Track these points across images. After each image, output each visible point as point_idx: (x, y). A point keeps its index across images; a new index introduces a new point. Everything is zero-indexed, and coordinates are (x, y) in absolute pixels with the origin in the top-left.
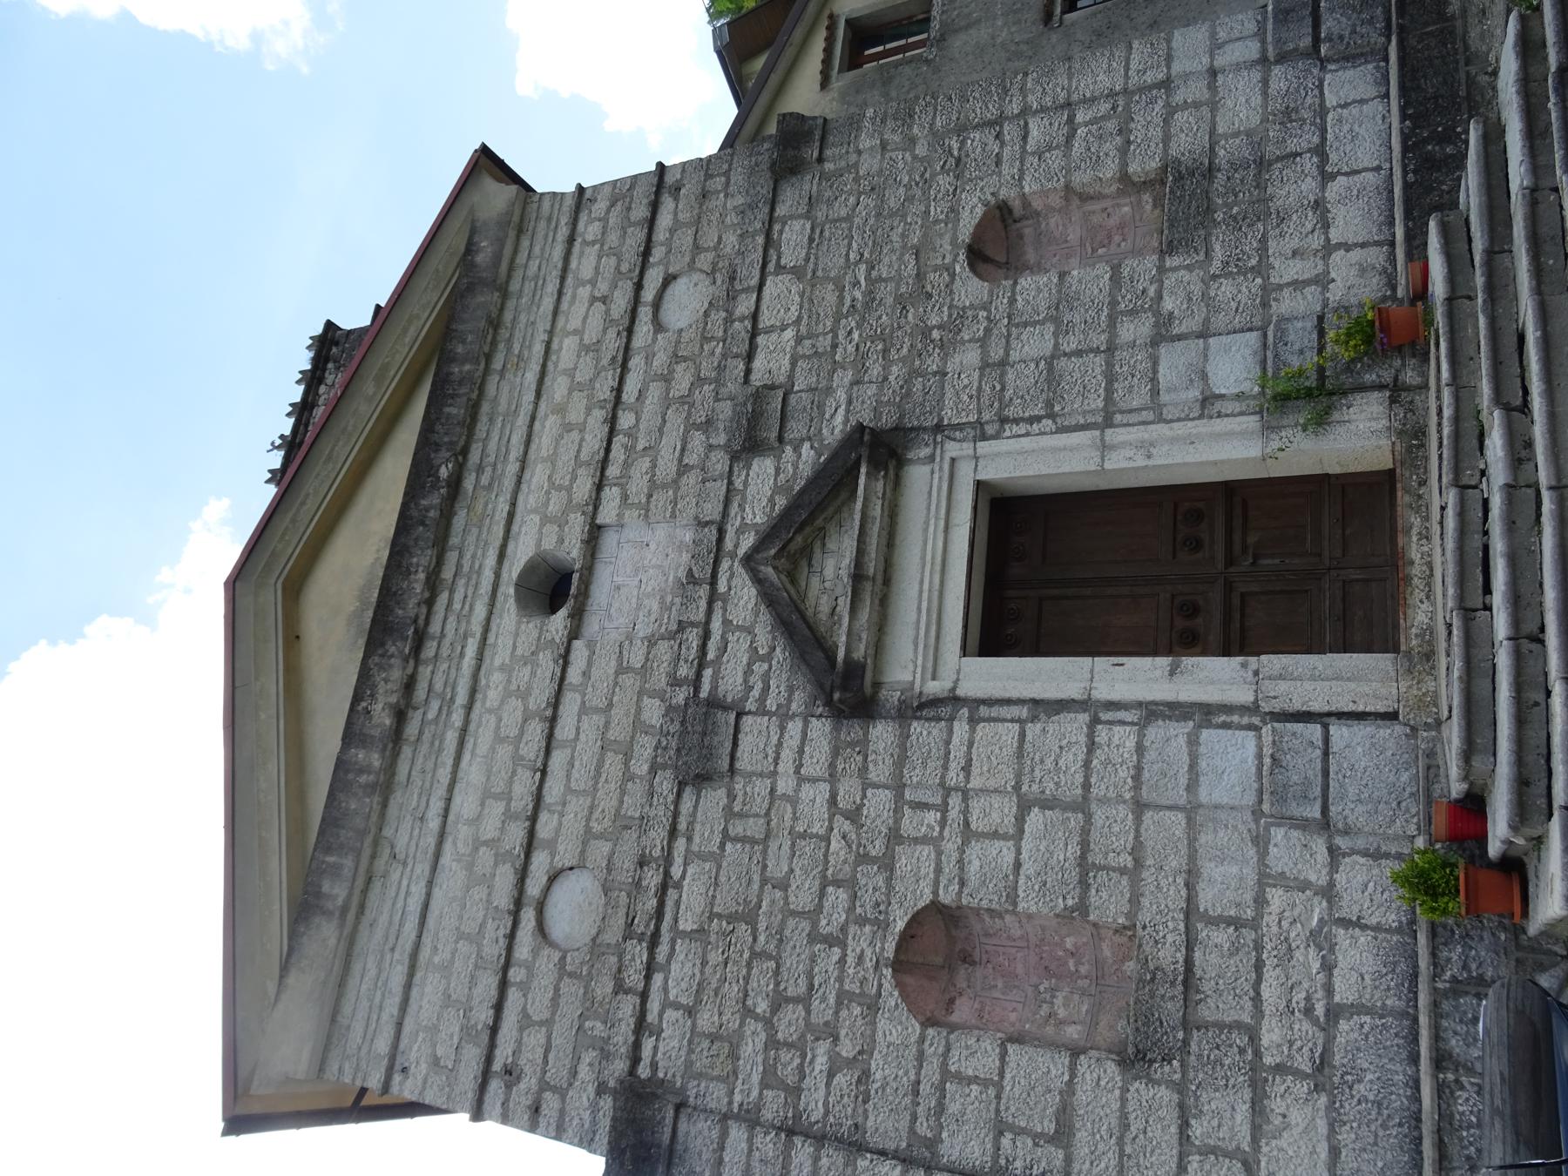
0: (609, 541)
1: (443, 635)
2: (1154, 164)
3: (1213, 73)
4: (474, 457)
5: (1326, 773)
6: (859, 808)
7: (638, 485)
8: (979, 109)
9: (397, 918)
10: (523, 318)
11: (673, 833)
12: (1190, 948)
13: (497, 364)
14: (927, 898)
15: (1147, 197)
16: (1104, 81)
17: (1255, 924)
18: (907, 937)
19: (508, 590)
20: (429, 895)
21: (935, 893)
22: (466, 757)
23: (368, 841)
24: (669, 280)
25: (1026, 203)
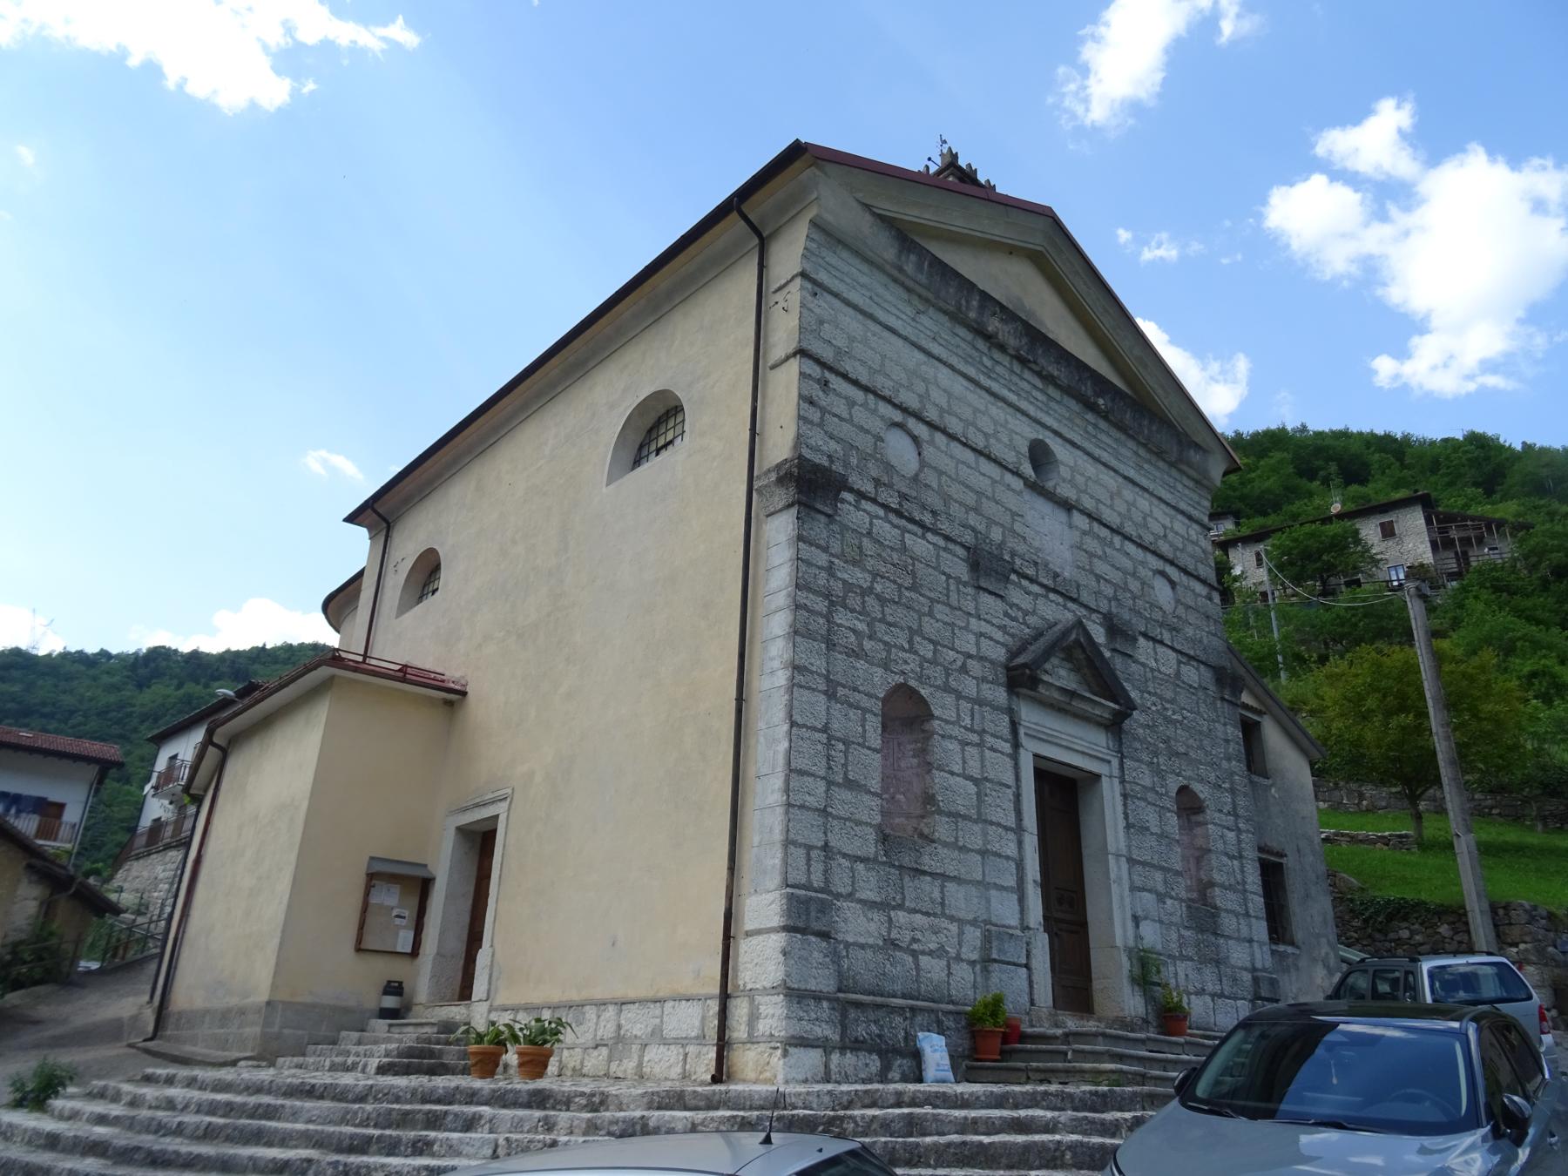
0: (1062, 515)
1: (1022, 379)
2: (1218, 903)
3: (1250, 941)
4: (1103, 424)
5: (1008, 963)
6: (967, 673)
7: (1092, 545)
8: (1241, 802)
9: (886, 305)
10: (1158, 474)
11: (947, 538)
12: (931, 874)
13: (1142, 452)
14: (937, 713)
15: (1195, 895)
16: (1250, 879)
17: (943, 915)
18: (913, 693)
19: (1043, 435)
20: (900, 336)
21: (938, 718)
22: (965, 383)
23: (931, 296)
24: (1173, 584)
25: (1199, 824)
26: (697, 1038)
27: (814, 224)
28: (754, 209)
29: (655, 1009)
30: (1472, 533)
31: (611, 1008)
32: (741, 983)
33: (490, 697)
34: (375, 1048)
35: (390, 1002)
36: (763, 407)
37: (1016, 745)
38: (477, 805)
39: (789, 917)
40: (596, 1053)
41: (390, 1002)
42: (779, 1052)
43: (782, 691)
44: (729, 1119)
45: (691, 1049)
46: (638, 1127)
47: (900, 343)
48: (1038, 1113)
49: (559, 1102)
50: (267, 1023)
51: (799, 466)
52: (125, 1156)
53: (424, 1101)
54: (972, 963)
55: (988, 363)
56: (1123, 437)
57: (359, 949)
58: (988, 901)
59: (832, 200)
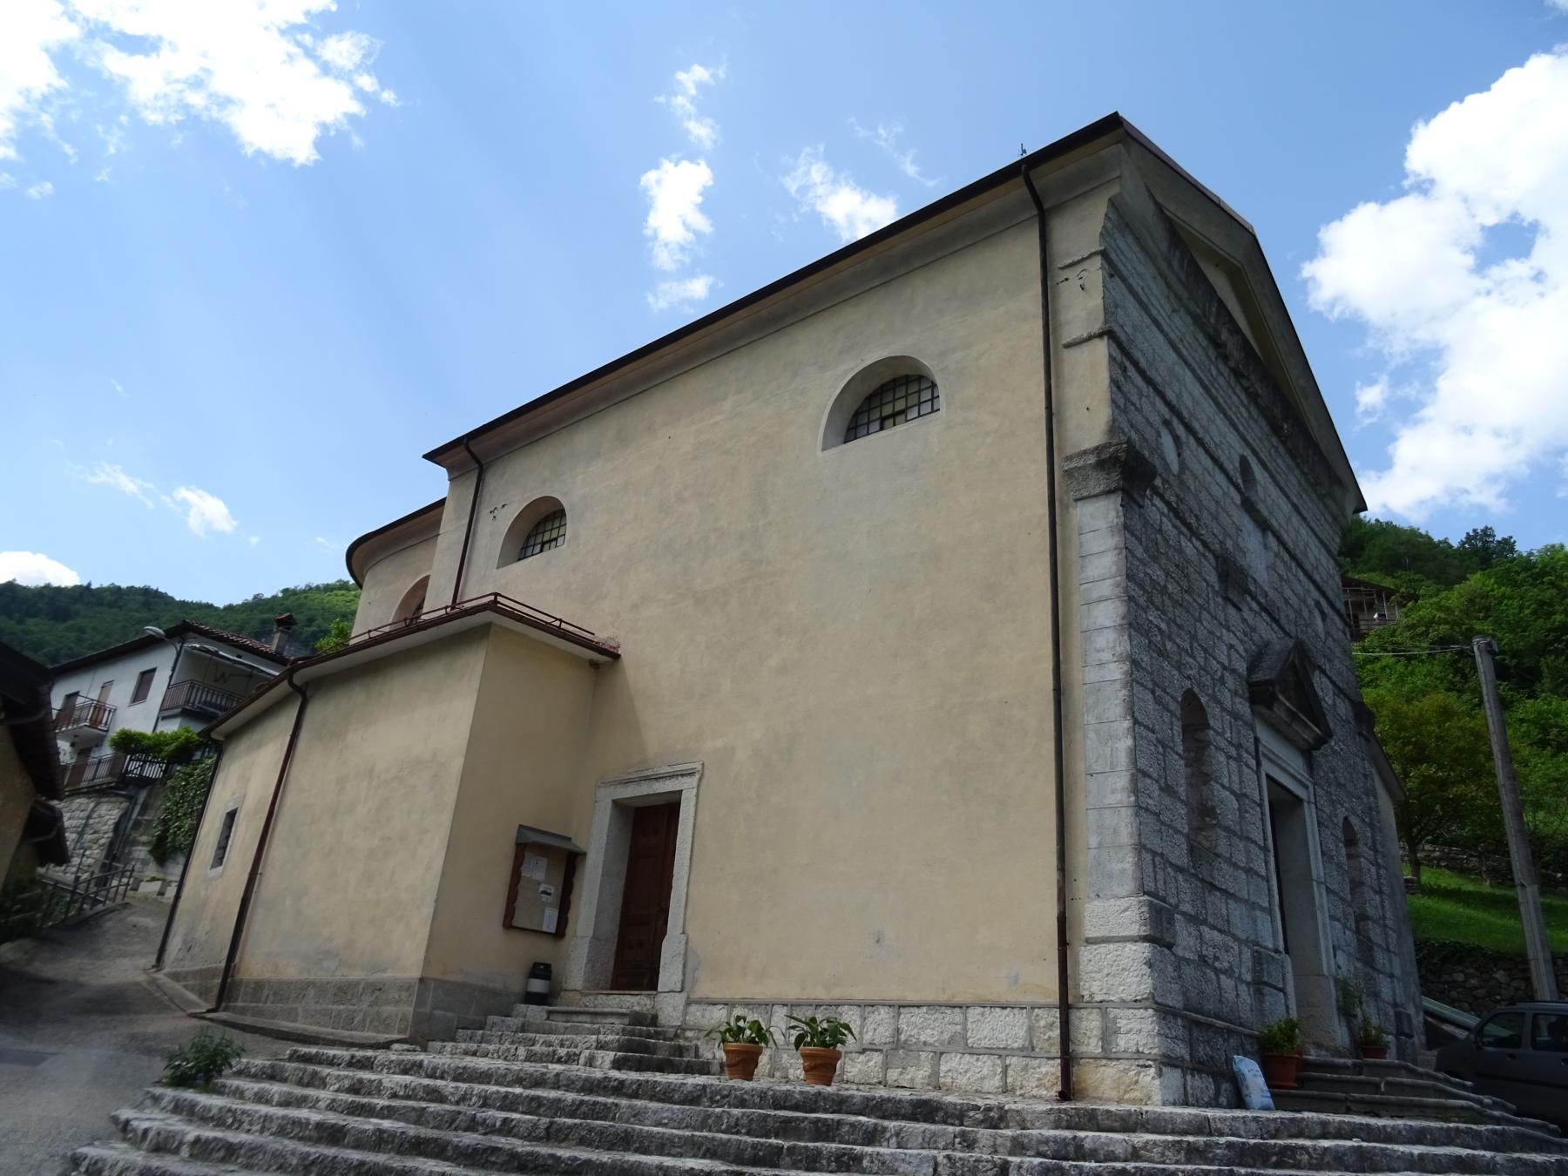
26: (1022, 1049)
27: (1112, 203)
28: (1045, 177)
29: (957, 1015)
30: (1364, 599)
31: (883, 1011)
32: (1086, 993)
33: (655, 660)
34: (578, 1038)
35: (538, 986)
36: (1057, 387)
37: (1259, 764)
38: (648, 779)
39: (1152, 928)
40: (862, 1058)
41: (538, 986)
42: (1152, 1071)
43: (1118, 686)
44: (1174, 1143)
45: (1012, 1061)
46: (1071, 1149)
47: (1161, 338)
48: (863, 1119)
49: (952, 1116)
50: (420, 1002)
51: (1127, 451)
52: (470, 1157)
53: (777, 1106)
54: (1248, 984)
55: (1214, 372)
56: (1292, 465)
57: (508, 923)
58: (1255, 921)
59: (1128, 184)
